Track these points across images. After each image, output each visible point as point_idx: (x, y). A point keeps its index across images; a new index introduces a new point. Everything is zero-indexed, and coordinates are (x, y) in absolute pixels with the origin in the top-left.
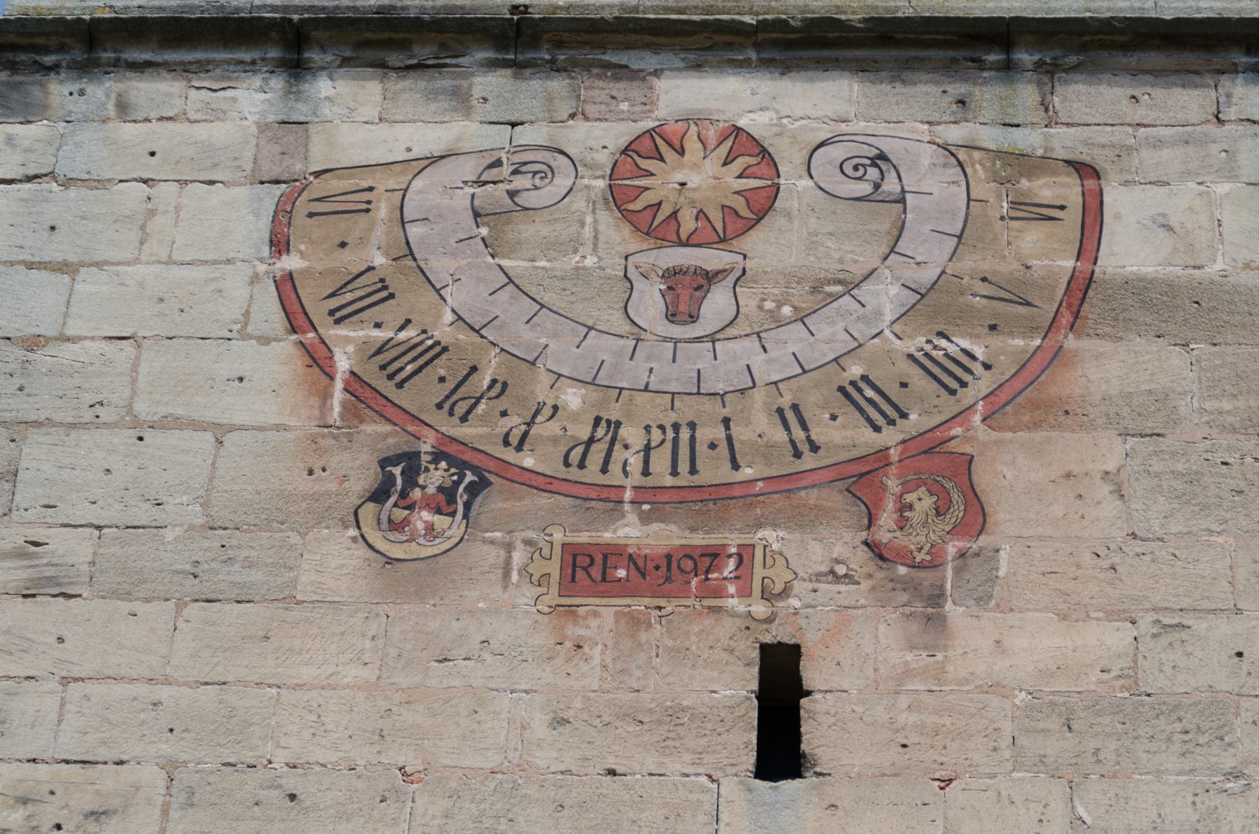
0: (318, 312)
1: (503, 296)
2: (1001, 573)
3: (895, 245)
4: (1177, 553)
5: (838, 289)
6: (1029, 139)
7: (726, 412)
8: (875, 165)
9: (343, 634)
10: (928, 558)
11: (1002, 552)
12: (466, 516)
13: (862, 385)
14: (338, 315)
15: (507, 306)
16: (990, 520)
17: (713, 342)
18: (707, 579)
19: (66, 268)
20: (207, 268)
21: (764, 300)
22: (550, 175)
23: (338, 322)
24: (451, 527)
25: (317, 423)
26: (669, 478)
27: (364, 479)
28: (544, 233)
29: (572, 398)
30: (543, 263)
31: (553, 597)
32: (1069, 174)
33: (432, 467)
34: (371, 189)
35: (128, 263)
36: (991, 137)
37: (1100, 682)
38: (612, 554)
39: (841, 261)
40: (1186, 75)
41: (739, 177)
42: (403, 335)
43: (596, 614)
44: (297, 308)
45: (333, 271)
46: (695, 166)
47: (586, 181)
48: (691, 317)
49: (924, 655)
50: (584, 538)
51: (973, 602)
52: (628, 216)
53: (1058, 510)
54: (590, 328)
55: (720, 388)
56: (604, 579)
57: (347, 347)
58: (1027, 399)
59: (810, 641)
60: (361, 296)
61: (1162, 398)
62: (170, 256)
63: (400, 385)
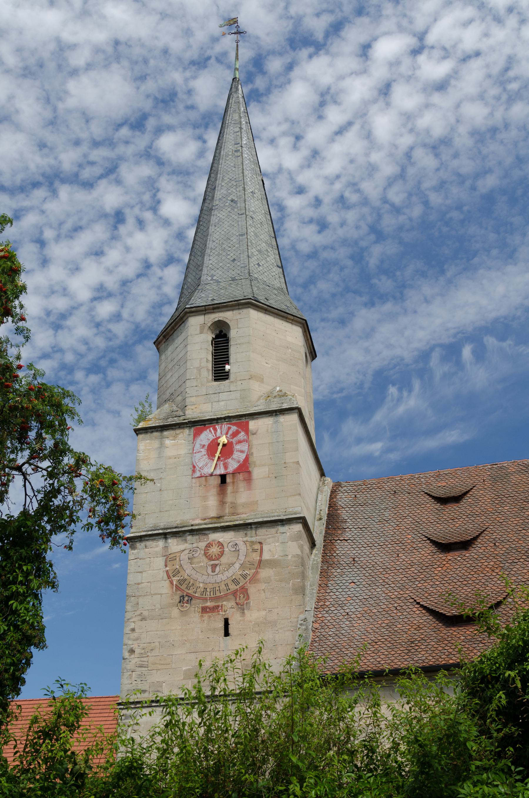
0: (171, 575)
6: (254, 539)
15: (193, 572)
19: (141, 572)
27: (178, 600)
29: (201, 585)
36: (249, 539)
38: (207, 607)
40: (273, 527)
52: (207, 557)
57: (175, 580)
58: (254, 579)
60: (176, 572)
61: (269, 577)
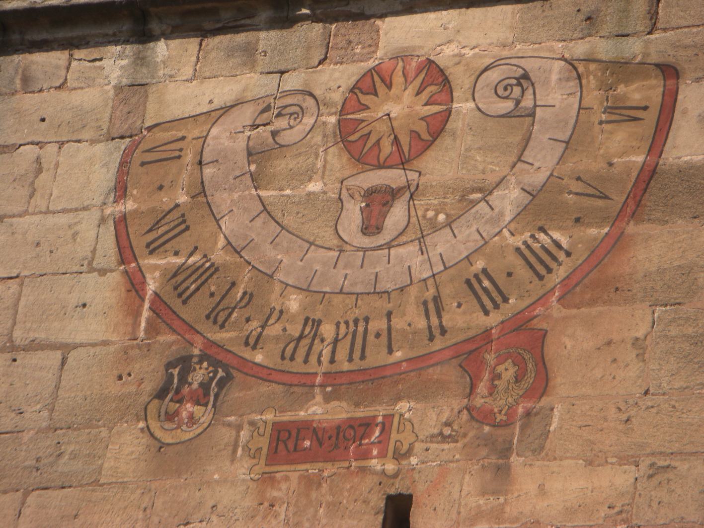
0: (139, 243)
1: (259, 222)
2: (552, 429)
3: (522, 154)
4: (677, 405)
5: (479, 195)
7: (390, 306)
8: (519, 84)
9: (125, 508)
10: (505, 418)
11: (555, 410)
12: (214, 406)
13: (482, 277)
14: (152, 247)
15: (262, 230)
16: (551, 384)
17: (389, 249)
18: (361, 445)
20: (71, 215)
21: (427, 210)
22: (300, 116)
23: (151, 253)
25: (129, 337)
26: (346, 363)
28: (291, 166)
29: (294, 303)
30: (288, 192)
32: (656, 77)
33: (198, 367)
34: (183, 138)
35: (20, 216)
37: (606, 517)
38: (305, 428)
39: (483, 172)
41: (426, 104)
42: (191, 260)
43: (287, 479)
44: (126, 244)
45: (153, 210)
46: (398, 99)
47: (324, 119)
48: (378, 229)
49: (492, 498)
50: (286, 417)
51: (530, 453)
53: (598, 373)
54: (311, 244)
55: (390, 286)
56: (295, 450)
57: (155, 269)
59: (419, 491)
60: (169, 228)
62: (48, 207)
63: (184, 302)
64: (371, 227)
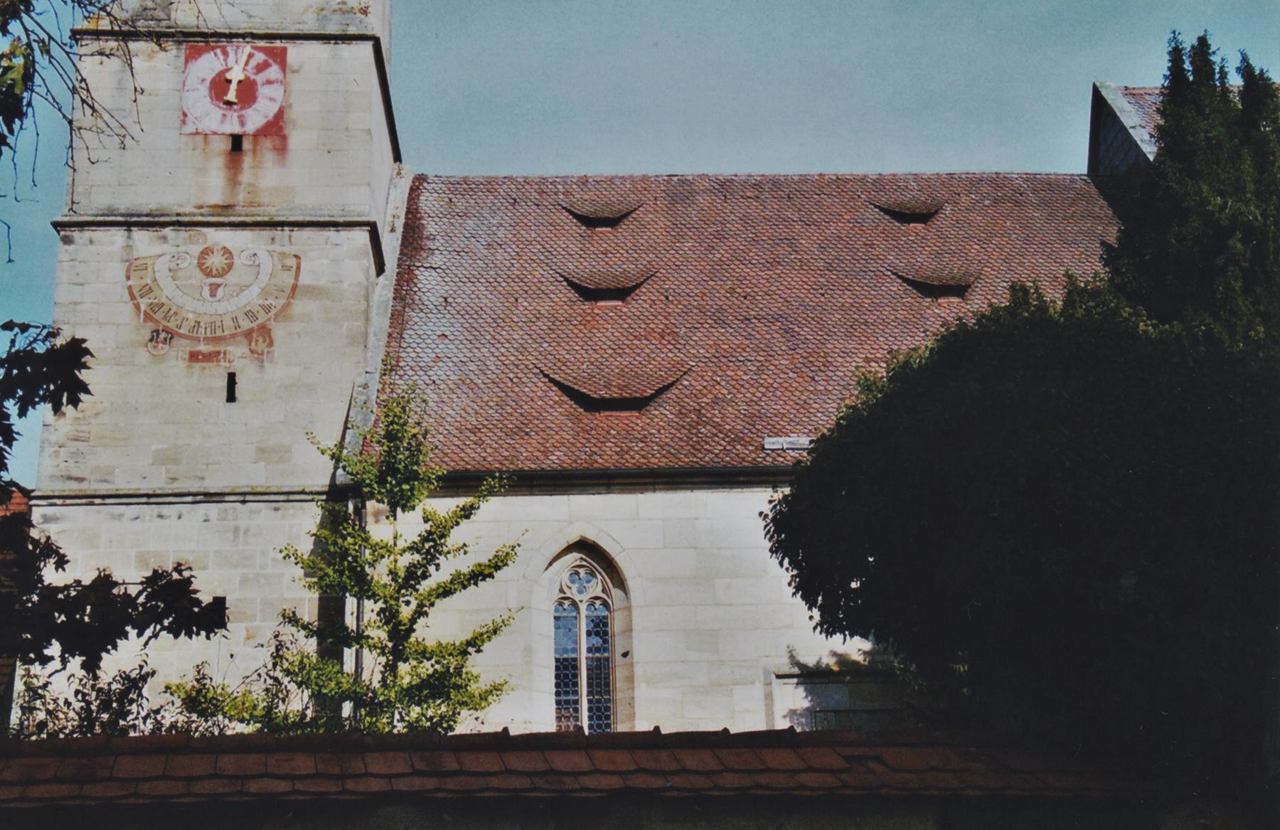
0: (137, 295)
19: (82, 284)
24: (167, 347)
27: (148, 336)
29: (191, 316)
31: (187, 363)
38: (199, 353)
57: (144, 304)
64: (213, 294)
